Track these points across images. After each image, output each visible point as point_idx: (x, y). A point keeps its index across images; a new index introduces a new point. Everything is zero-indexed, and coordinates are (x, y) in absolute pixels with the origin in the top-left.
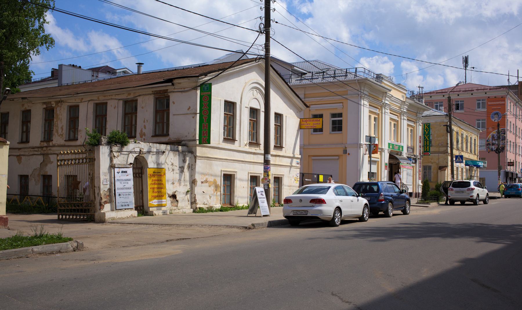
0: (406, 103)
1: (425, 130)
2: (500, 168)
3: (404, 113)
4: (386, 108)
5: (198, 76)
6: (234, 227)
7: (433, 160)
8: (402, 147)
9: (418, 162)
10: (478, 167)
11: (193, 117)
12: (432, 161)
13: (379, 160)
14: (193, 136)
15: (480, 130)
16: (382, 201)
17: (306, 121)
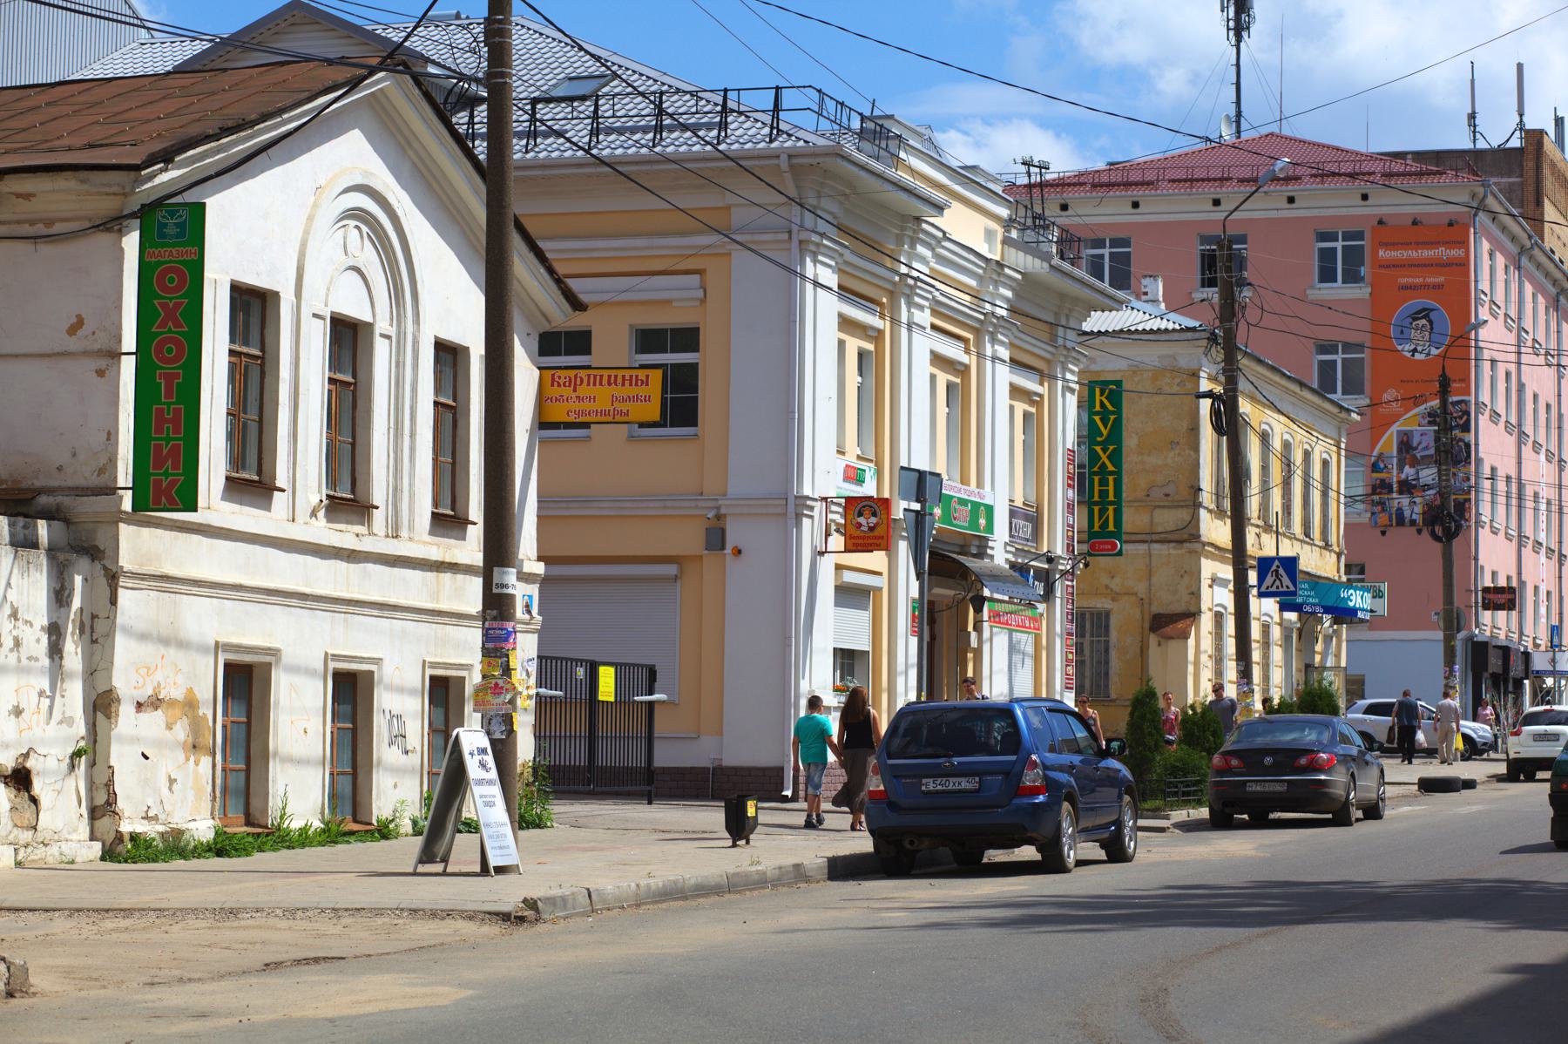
0: (1007, 271)
1: (1097, 418)
2: (1452, 621)
3: (995, 326)
4: (917, 299)
5: (137, 168)
6: (449, 914)
7: (1117, 580)
8: (990, 510)
9: (1058, 594)
10: (1344, 615)
11: (101, 373)
12: (1116, 584)
13: (881, 582)
14: (101, 471)
15: (1348, 411)
16: (1035, 791)
17: (574, 384)
